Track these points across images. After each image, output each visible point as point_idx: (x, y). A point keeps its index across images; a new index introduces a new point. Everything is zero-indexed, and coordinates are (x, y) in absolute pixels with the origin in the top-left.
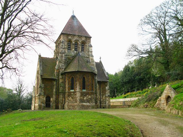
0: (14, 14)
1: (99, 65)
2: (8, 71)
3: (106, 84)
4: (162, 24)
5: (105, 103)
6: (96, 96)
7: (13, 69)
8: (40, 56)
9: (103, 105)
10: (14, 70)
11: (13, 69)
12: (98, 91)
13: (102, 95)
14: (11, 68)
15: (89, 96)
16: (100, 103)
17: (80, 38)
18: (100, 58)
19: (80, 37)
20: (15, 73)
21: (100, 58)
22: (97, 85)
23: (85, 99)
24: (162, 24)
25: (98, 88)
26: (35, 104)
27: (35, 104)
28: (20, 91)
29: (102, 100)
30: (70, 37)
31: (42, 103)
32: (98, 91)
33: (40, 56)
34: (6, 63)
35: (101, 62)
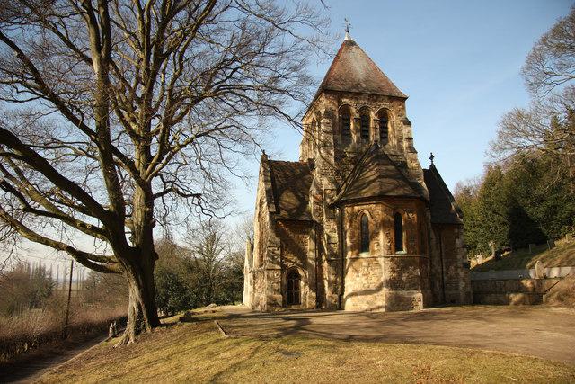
0: (76, 147)
1: (432, 174)
2: (180, 200)
3: (456, 231)
4: (275, 79)
5: (457, 289)
6: (432, 266)
7: (194, 195)
8: (264, 156)
9: (450, 293)
10: (196, 199)
11: (194, 195)
12: (435, 253)
13: (446, 263)
14: (187, 193)
15: (415, 269)
16: (443, 287)
17: (375, 101)
18: (432, 157)
19: (375, 98)
20: (198, 208)
21: (432, 157)
22: (432, 235)
23: (404, 278)
24: (275, 79)
25: (434, 242)
26: (253, 295)
27: (253, 295)
28: (211, 254)
29: (446, 278)
30: (346, 101)
31: (276, 291)
32: (435, 253)
33: (264, 156)
34: (173, 179)
35: (433, 167)
